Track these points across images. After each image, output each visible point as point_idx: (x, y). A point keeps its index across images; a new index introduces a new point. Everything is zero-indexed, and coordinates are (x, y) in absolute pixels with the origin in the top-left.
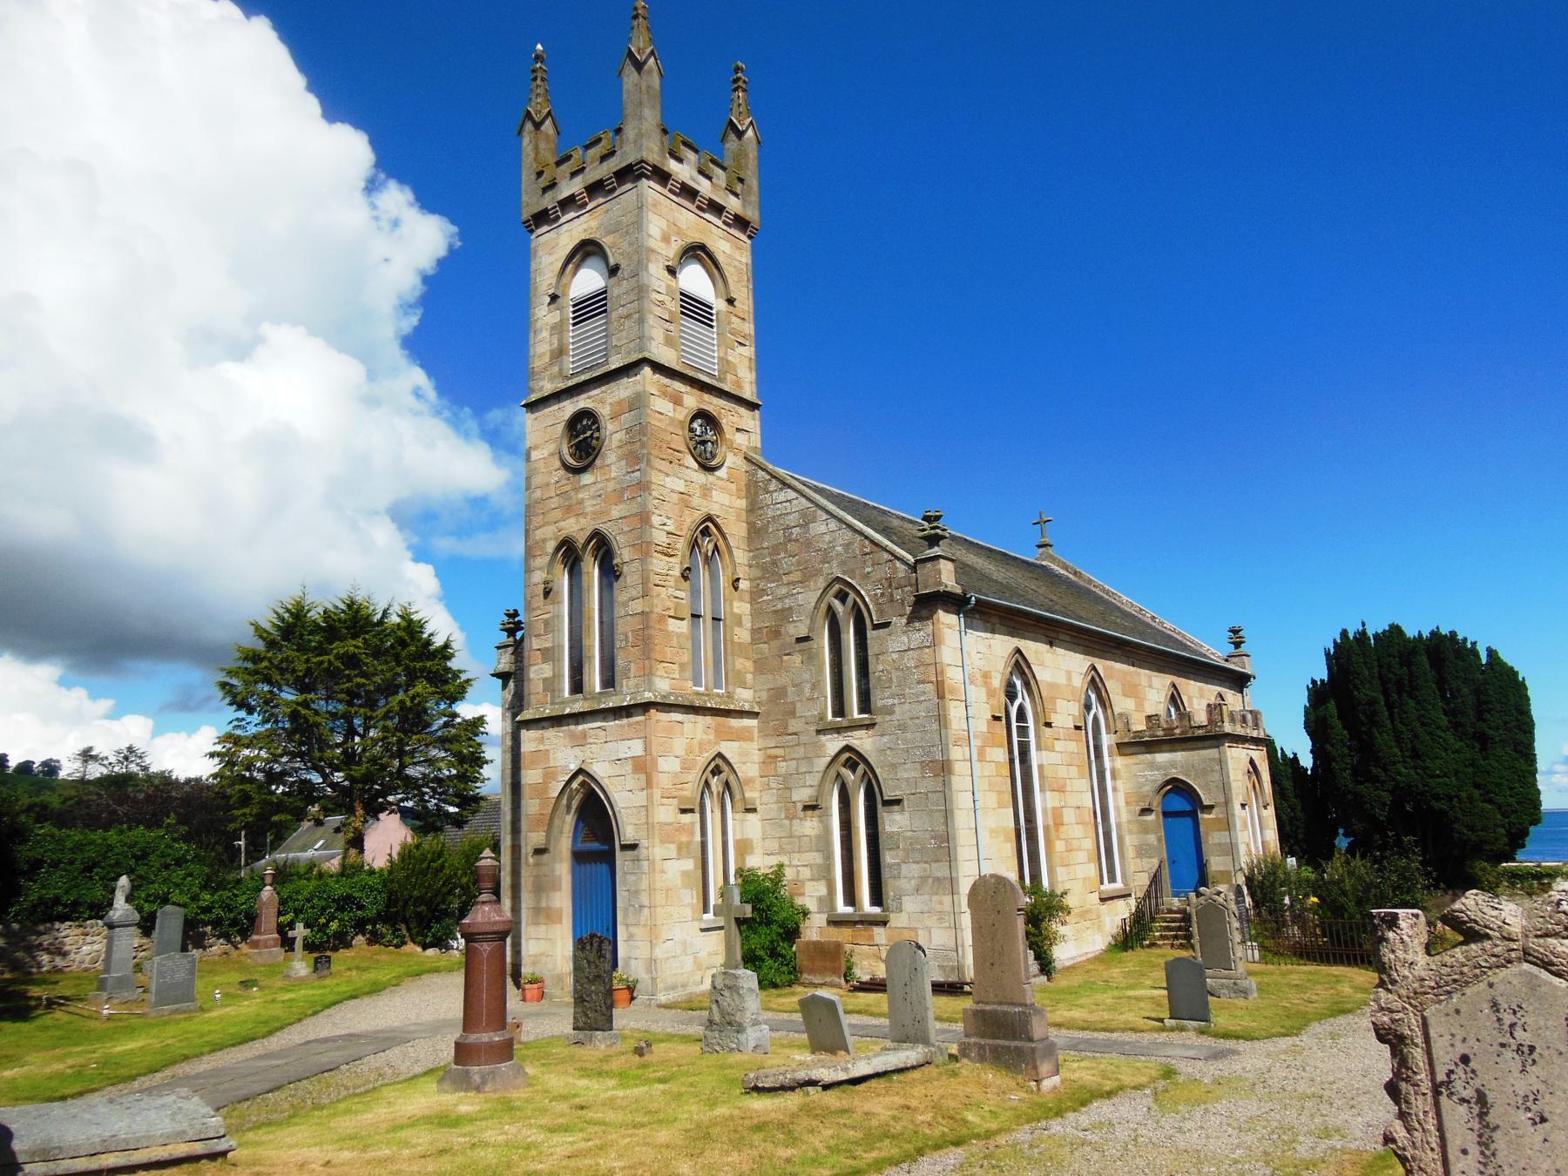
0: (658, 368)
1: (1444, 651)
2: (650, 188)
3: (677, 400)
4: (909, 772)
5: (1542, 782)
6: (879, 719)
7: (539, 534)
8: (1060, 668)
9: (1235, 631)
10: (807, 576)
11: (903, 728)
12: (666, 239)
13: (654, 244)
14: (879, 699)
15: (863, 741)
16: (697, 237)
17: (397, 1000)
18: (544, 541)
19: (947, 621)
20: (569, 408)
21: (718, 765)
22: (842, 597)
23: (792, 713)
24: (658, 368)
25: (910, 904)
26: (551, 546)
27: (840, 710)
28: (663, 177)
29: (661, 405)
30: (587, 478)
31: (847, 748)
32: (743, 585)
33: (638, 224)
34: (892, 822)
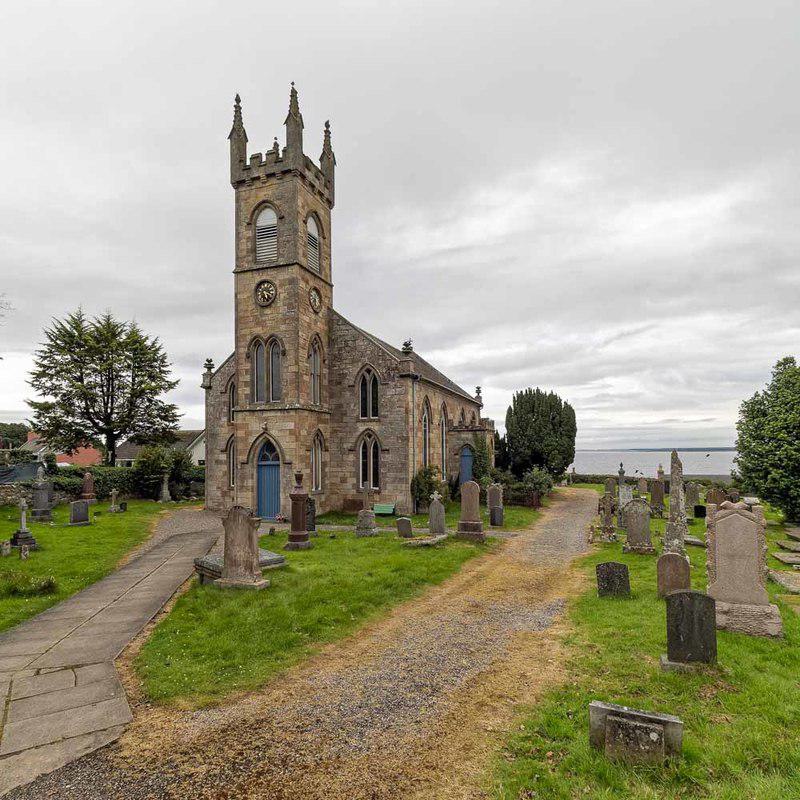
0: (302, 267)
1: (553, 400)
2: (299, 181)
3: (307, 282)
4: (393, 439)
5: (577, 440)
6: (382, 419)
7: (243, 332)
8: (437, 402)
9: (478, 388)
10: (353, 362)
11: (391, 423)
12: (303, 207)
13: (300, 210)
14: (382, 412)
15: (375, 427)
16: (314, 207)
17: (615, 604)
18: (245, 335)
19: (409, 382)
20: (258, 278)
21: (319, 434)
22: (369, 371)
23: (345, 414)
24: (302, 267)
25: (389, 487)
26: (249, 338)
27: (364, 414)
28: (303, 177)
29: (302, 284)
30: (268, 311)
31: (368, 429)
32: (326, 362)
33: (294, 199)
34: (384, 458)
